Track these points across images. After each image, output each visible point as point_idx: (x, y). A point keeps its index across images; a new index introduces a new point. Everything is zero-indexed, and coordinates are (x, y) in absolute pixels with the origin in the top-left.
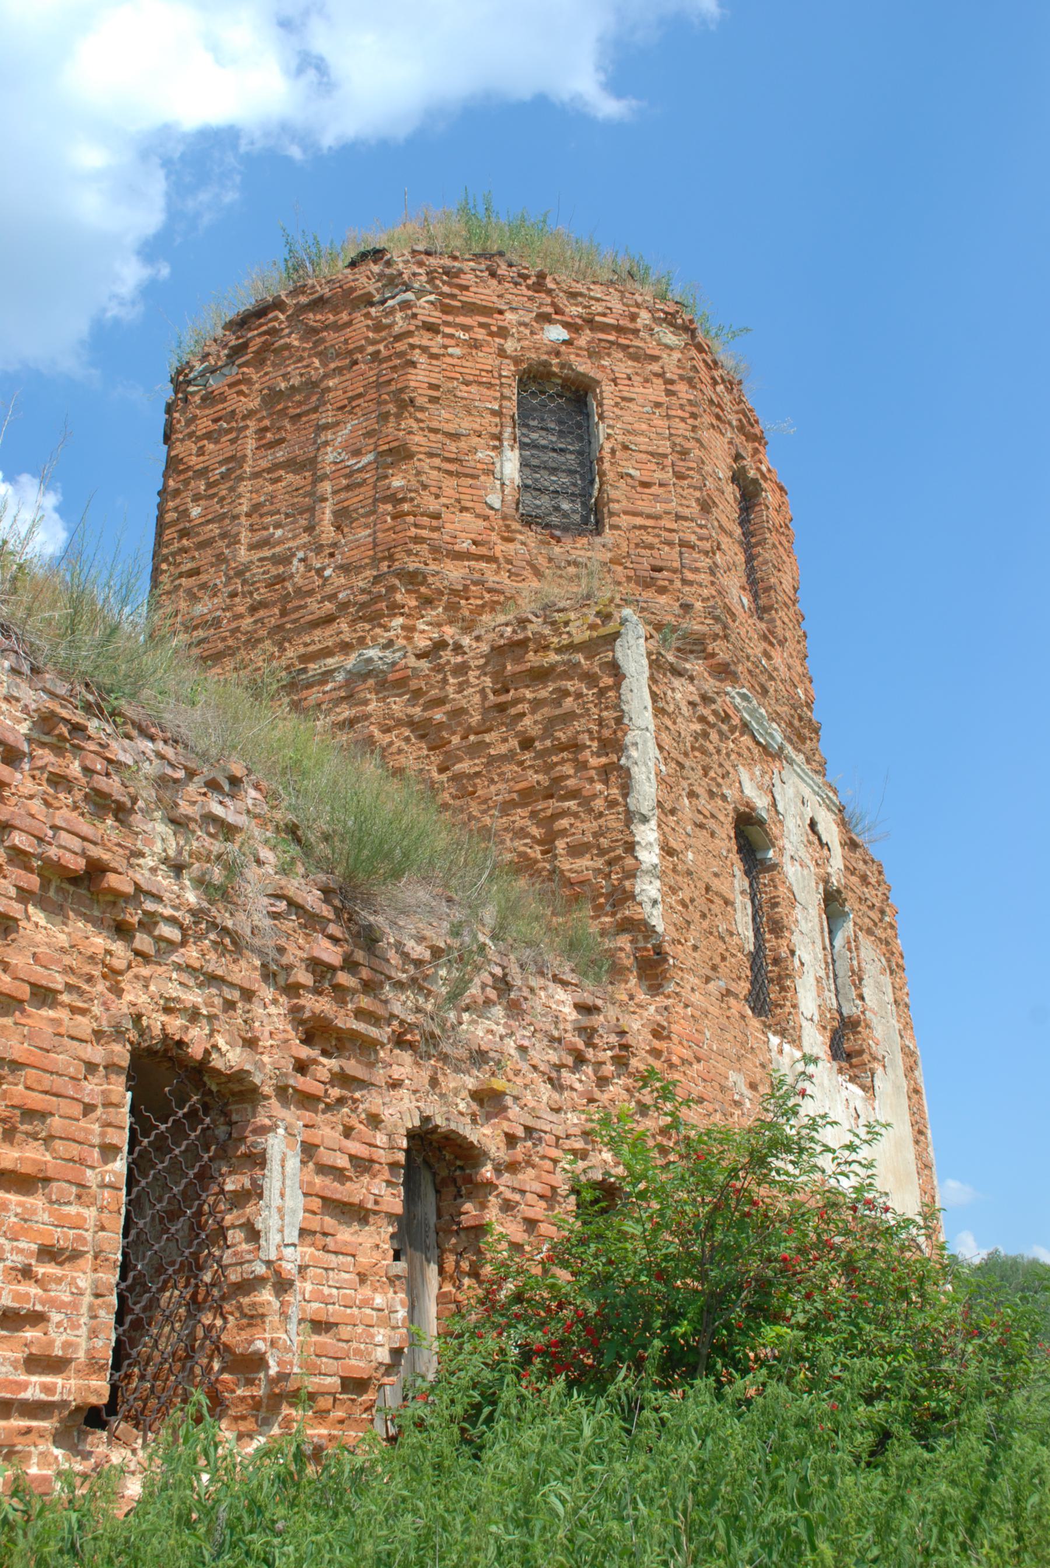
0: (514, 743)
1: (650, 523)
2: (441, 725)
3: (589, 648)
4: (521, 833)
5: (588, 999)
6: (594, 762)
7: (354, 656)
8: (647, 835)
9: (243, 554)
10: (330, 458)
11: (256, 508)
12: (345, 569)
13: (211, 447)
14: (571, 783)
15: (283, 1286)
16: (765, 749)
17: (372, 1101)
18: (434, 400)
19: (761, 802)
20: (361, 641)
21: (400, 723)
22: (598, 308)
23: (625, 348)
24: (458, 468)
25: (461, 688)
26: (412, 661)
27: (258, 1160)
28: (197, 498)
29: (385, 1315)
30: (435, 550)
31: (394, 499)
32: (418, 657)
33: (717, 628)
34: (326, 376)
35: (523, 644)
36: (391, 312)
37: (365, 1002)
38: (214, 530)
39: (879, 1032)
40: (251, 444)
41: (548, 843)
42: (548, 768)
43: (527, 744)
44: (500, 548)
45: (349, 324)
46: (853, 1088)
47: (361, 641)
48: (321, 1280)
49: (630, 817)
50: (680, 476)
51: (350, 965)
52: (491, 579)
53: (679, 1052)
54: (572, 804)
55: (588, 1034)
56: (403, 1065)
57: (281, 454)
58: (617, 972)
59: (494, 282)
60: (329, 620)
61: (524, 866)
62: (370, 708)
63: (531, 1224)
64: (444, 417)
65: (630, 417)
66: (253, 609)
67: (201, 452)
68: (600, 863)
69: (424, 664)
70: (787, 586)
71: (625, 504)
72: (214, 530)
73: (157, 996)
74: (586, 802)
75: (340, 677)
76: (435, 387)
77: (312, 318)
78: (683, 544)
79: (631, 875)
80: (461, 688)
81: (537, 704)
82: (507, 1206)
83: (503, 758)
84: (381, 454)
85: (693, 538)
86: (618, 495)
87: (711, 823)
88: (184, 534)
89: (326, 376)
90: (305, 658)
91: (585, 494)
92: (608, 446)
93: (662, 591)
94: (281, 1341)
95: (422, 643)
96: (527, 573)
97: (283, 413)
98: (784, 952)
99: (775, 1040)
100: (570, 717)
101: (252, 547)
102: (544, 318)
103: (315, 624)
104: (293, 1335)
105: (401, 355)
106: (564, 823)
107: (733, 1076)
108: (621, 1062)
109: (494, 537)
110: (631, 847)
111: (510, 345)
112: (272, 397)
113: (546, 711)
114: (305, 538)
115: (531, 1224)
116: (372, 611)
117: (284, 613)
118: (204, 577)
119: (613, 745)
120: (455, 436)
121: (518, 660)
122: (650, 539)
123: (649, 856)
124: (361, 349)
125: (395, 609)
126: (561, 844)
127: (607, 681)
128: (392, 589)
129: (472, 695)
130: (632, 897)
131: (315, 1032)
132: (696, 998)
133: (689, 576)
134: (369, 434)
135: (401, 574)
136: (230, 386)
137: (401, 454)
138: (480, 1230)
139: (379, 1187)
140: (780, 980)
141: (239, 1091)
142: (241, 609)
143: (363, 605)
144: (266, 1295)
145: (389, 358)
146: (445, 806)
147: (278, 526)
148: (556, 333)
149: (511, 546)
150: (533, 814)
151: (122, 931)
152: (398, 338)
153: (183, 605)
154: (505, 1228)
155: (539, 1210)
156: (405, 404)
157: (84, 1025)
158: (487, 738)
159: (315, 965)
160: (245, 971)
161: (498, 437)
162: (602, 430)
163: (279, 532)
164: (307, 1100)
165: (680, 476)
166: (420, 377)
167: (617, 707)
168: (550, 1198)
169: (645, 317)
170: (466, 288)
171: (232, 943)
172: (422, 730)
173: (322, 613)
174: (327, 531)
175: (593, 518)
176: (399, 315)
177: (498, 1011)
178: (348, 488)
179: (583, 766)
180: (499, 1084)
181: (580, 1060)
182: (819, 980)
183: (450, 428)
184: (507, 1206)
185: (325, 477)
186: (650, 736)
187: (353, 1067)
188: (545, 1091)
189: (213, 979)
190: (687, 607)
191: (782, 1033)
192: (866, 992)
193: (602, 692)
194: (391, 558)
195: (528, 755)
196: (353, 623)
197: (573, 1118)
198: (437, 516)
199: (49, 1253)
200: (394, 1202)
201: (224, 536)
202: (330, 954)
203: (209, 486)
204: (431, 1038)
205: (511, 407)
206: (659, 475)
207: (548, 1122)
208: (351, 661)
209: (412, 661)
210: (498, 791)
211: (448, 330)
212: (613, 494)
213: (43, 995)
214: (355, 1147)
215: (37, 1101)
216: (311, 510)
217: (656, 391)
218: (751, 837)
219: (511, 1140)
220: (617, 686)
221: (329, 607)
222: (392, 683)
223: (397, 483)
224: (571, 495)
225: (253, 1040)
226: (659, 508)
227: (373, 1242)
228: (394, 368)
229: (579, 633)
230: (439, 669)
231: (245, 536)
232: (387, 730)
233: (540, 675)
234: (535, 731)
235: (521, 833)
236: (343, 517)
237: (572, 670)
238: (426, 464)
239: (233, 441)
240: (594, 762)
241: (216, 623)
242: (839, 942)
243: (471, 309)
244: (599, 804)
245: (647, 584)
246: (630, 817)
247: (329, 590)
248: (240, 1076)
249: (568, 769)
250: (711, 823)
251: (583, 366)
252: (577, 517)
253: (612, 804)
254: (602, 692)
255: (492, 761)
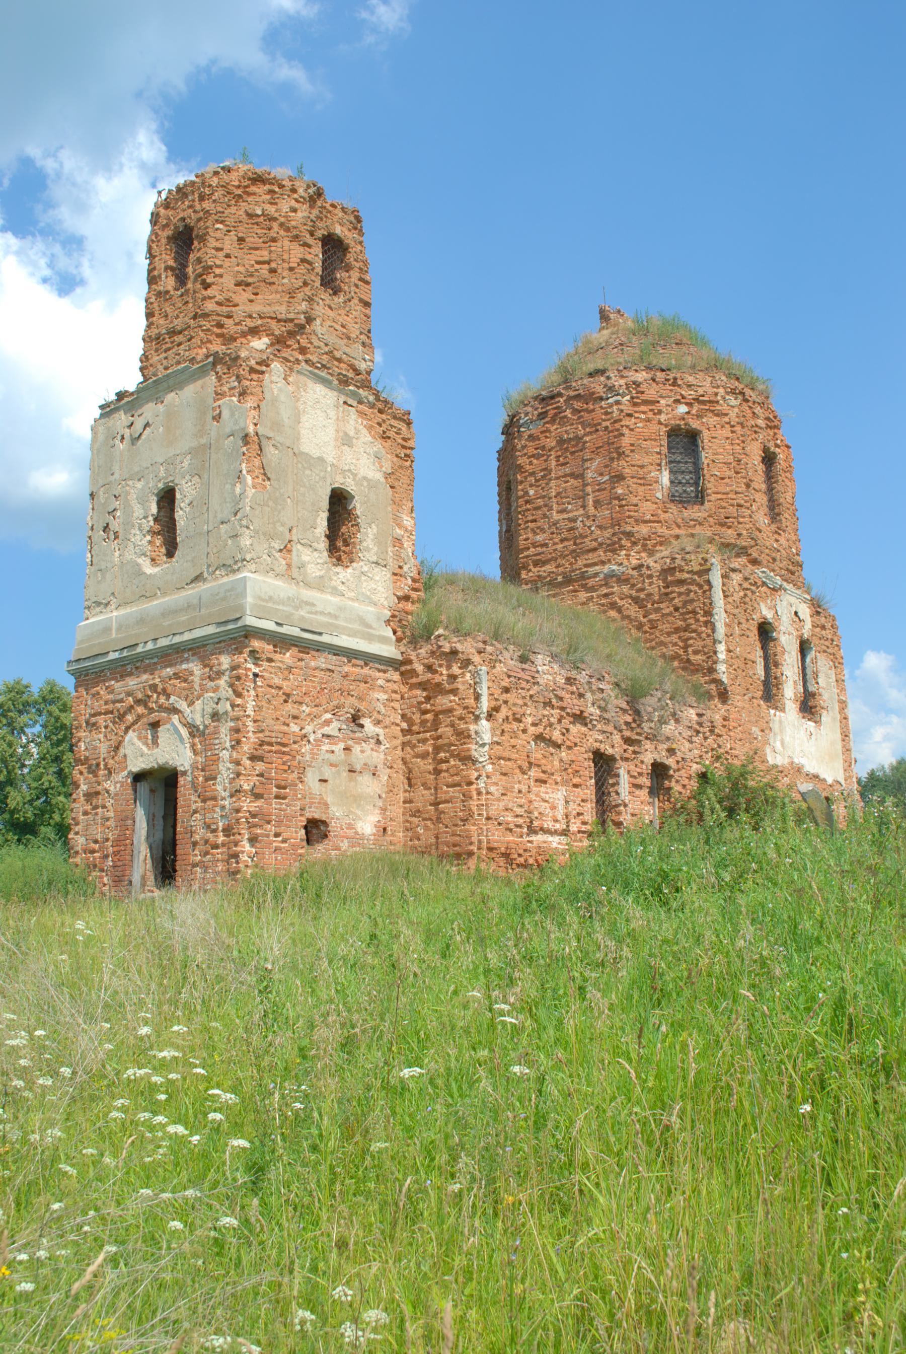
0: (672, 609)
1: (724, 497)
2: (643, 600)
3: (700, 573)
4: (675, 644)
5: (700, 711)
6: (702, 619)
7: (607, 566)
8: (721, 648)
9: (555, 516)
10: (590, 475)
11: (558, 494)
12: (600, 527)
13: (535, 461)
14: (693, 627)
15: (625, 805)
16: (774, 589)
17: (641, 757)
18: (632, 451)
19: (769, 615)
20: (609, 561)
21: (627, 597)
22: (701, 391)
23: (713, 411)
24: (645, 482)
25: (651, 584)
26: (630, 572)
27: (618, 776)
28: (531, 486)
29: (648, 812)
30: (636, 521)
31: (618, 498)
32: (633, 569)
33: (753, 543)
34: (585, 435)
35: (674, 568)
36: (611, 406)
37: (638, 730)
38: (540, 502)
39: (826, 696)
40: (554, 463)
41: (686, 648)
42: (685, 620)
43: (677, 609)
44: (663, 516)
45: (593, 410)
46: (810, 723)
47: (609, 561)
48: (636, 804)
49: (715, 642)
50: (737, 473)
51: (634, 721)
52: (660, 530)
53: (732, 724)
54: (693, 635)
55: (700, 724)
56: (648, 745)
57: (568, 470)
58: (711, 698)
59: (654, 385)
60: (595, 550)
61: (676, 657)
62: (615, 589)
63: (684, 786)
64: (637, 458)
65: (714, 450)
66: (562, 541)
67: (531, 463)
68: (704, 658)
69: (635, 573)
70: (789, 499)
71: (714, 489)
72: (540, 502)
73: (593, 739)
74: (699, 634)
75: (602, 576)
76: (632, 445)
77: (577, 405)
78: (739, 505)
79: (715, 663)
80: (651, 584)
81: (680, 594)
82: (677, 781)
83: (667, 614)
84: (612, 477)
85: (742, 502)
86: (710, 485)
87: (748, 633)
88: (527, 502)
89: (585, 435)
90: (586, 566)
91: (696, 484)
92: (706, 462)
93: (729, 527)
94: (626, 818)
95: (635, 562)
96: (674, 526)
97: (566, 449)
98: (779, 674)
99: (772, 712)
100: (692, 601)
101: (558, 512)
102: (677, 401)
103: (589, 551)
104: (629, 817)
105: (618, 430)
106: (691, 642)
107: (754, 729)
108: (712, 731)
109: (660, 512)
110: (715, 652)
111: (663, 418)
112: (561, 442)
113: (683, 597)
114: (581, 512)
115: (684, 786)
116: (613, 548)
117: (575, 544)
118: (539, 524)
119: (709, 613)
120: (642, 467)
121: (672, 575)
122: (724, 504)
123: (722, 656)
124: (600, 424)
125: (622, 547)
126: (690, 650)
127: (706, 587)
128: (620, 539)
129: (655, 587)
130: (715, 670)
131: (628, 741)
132: (740, 704)
133: (741, 520)
134: (606, 466)
135: (624, 533)
136: (542, 432)
137: (620, 478)
138: (670, 789)
139: (644, 780)
140: (777, 685)
141: (612, 759)
142: (557, 540)
143: (609, 545)
144: (622, 808)
145: (612, 431)
146: (646, 632)
147: (569, 503)
148: (683, 409)
149: (667, 515)
150: (680, 638)
151: (586, 725)
152: (615, 422)
153: (530, 535)
154: (677, 788)
155: (686, 782)
156: (621, 454)
157: (583, 750)
158: (662, 606)
159: (627, 723)
160: (610, 728)
161: (659, 465)
162: (703, 454)
163: (570, 507)
164: (627, 759)
165: (737, 473)
166: (626, 441)
167: (710, 598)
168: (690, 778)
169: (721, 391)
170: (643, 393)
171: (607, 721)
172: (636, 600)
173: (591, 547)
174: (591, 510)
175: (700, 497)
176: (615, 407)
177: (672, 722)
178: (599, 490)
179: (697, 620)
180: (674, 746)
181: (698, 732)
182: (795, 682)
183: (639, 463)
184: (677, 781)
185: (588, 484)
186: (722, 610)
187: (636, 748)
188: (687, 745)
189: (604, 732)
190: (739, 535)
191: (776, 708)
192: (820, 680)
193: (704, 592)
194: (619, 525)
195: (677, 614)
196: (605, 552)
197: (696, 752)
198: (636, 505)
199: (583, 801)
200: (648, 783)
201: (546, 506)
202: (629, 719)
203: (537, 481)
204: (655, 736)
205: (665, 450)
206: (728, 473)
207: (689, 756)
208: (606, 569)
209: (630, 572)
210: (666, 627)
211: (637, 415)
212: (709, 485)
213: (576, 745)
214: (639, 770)
215: (578, 768)
216: (583, 498)
217: (726, 432)
218: (765, 631)
219: (678, 762)
220: (710, 590)
221: (594, 544)
222: (622, 580)
223: (620, 491)
224: (691, 490)
225: (614, 747)
226: (728, 489)
227: (644, 794)
228: (615, 437)
229: (697, 568)
230: (641, 575)
231: (555, 507)
232: (622, 599)
233: (681, 582)
234: (680, 605)
235: (675, 644)
236: (597, 504)
237: (693, 582)
238: (630, 482)
239: (546, 461)
240: (702, 619)
241: (546, 545)
242: (808, 660)
243: (646, 402)
244: (704, 635)
245: (722, 525)
246: (715, 642)
247: (594, 536)
248: (613, 756)
249: (692, 621)
250: (748, 633)
251: (695, 424)
252: (693, 495)
253: (709, 636)
254: (704, 592)
255: (663, 615)
